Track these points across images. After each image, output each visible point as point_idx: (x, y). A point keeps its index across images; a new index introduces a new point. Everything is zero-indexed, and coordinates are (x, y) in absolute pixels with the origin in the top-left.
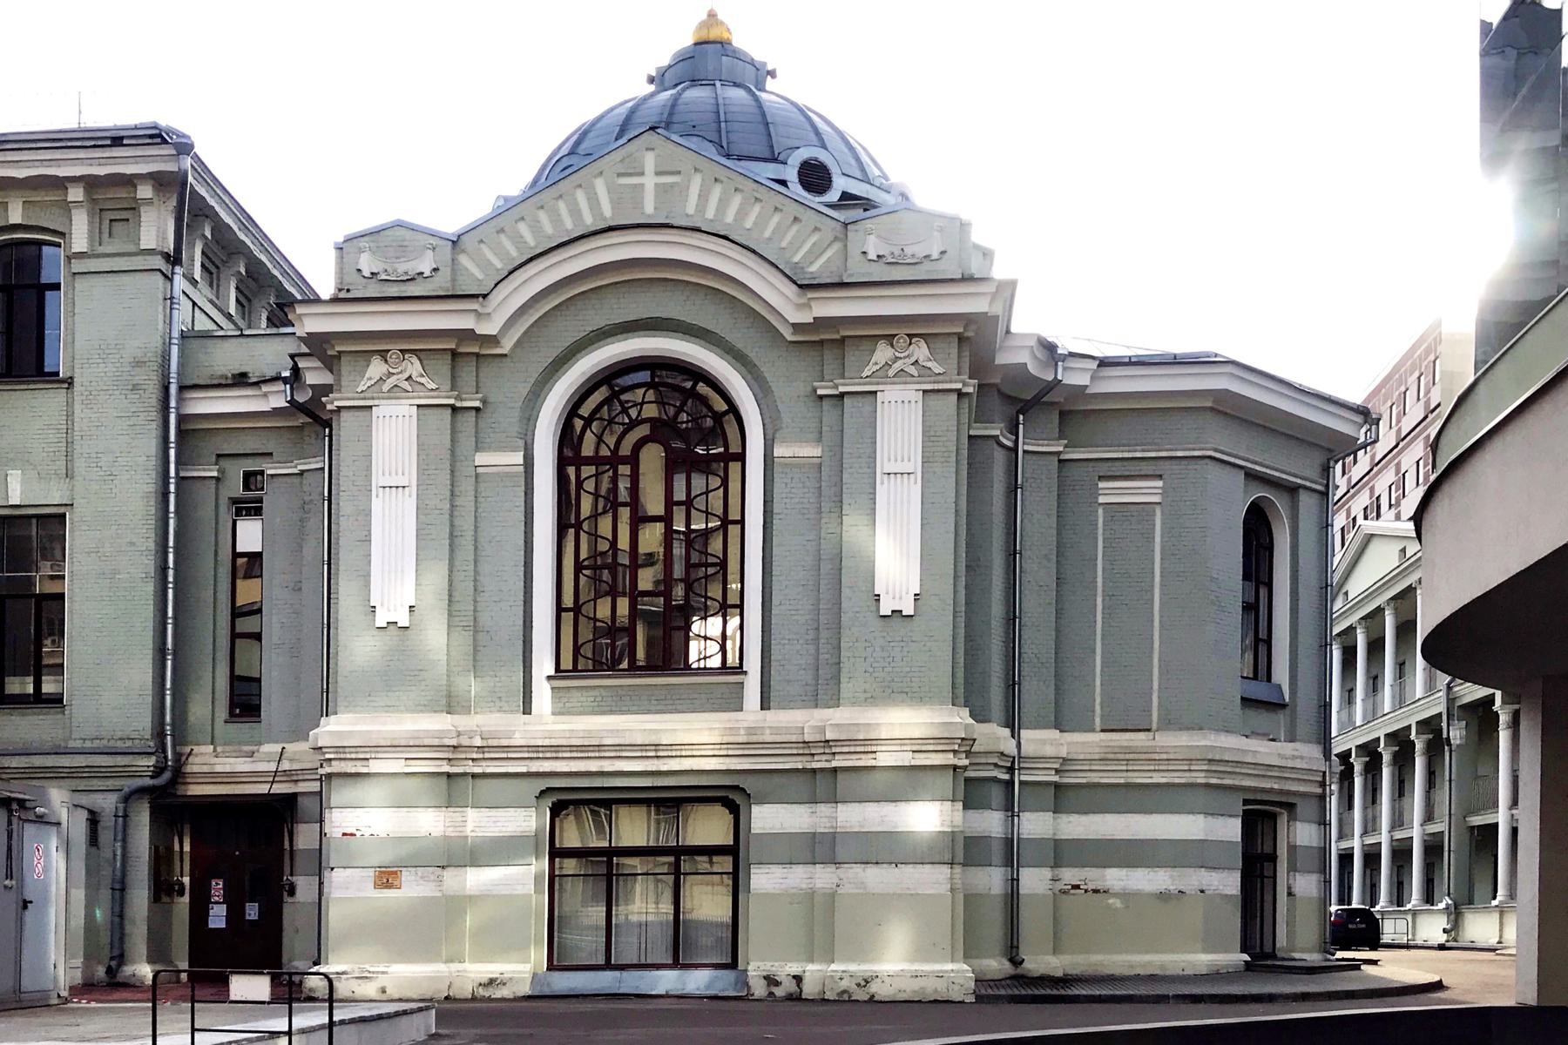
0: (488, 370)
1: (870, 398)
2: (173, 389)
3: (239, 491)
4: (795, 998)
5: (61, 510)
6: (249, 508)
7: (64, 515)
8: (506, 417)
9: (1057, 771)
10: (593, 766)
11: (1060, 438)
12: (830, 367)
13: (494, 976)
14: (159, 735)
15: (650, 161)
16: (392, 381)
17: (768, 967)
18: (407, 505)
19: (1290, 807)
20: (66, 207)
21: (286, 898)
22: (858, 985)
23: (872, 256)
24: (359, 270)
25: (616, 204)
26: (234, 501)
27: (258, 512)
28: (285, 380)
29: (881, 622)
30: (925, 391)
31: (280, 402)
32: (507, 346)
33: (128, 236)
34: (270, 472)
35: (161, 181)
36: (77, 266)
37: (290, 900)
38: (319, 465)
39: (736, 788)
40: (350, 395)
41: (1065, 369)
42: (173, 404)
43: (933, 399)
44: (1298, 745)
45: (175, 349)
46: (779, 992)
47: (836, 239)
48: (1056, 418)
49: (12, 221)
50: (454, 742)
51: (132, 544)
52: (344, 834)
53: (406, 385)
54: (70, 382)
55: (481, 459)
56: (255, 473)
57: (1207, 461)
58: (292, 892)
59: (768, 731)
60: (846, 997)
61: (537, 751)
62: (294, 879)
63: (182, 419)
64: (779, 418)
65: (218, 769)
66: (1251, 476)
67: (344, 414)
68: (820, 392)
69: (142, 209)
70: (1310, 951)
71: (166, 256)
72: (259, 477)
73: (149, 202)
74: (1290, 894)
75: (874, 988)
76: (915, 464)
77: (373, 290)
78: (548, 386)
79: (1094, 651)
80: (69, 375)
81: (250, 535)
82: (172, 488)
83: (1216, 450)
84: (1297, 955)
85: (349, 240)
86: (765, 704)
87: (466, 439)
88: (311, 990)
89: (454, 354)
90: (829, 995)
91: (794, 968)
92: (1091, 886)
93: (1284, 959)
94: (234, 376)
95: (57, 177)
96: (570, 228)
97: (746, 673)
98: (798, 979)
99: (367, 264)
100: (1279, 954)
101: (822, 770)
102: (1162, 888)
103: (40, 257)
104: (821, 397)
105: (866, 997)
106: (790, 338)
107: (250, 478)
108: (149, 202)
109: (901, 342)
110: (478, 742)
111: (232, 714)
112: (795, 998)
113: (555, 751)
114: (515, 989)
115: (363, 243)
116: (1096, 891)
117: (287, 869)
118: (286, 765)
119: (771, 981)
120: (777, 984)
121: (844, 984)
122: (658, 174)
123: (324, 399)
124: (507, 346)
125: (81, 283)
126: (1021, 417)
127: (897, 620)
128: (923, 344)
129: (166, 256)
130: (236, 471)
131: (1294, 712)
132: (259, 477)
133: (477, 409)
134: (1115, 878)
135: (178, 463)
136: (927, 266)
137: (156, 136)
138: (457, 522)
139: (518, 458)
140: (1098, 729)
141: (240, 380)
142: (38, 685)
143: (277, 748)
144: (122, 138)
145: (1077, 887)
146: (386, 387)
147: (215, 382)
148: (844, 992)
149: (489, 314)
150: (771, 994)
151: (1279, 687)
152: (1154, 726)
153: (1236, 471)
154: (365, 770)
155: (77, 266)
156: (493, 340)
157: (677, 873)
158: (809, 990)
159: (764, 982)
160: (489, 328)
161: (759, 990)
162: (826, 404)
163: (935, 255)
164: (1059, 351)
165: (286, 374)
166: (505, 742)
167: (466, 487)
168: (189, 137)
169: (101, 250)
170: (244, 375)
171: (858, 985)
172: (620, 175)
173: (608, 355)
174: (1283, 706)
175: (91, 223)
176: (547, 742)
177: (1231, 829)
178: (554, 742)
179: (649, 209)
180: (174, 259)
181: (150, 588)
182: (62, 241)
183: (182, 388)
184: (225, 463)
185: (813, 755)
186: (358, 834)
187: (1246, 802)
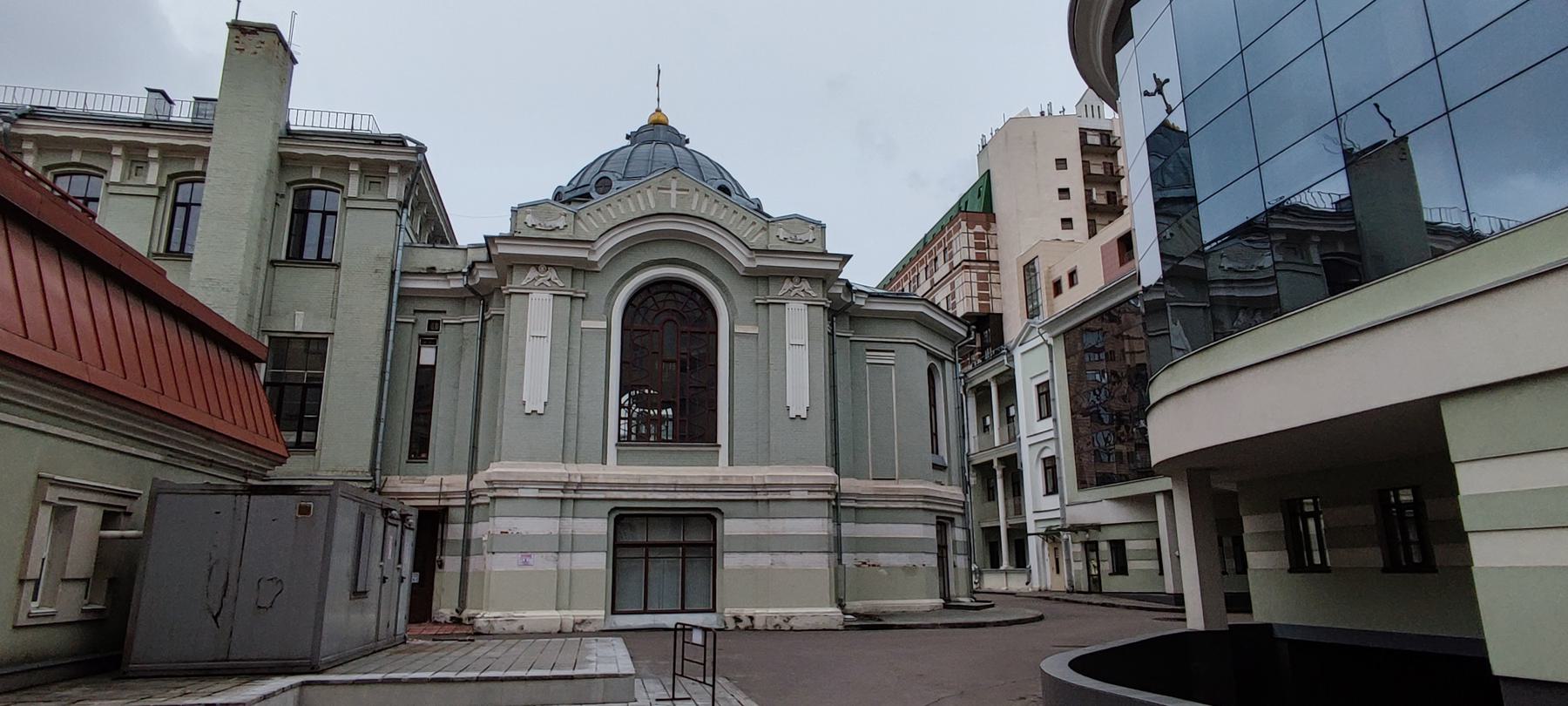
0: (590, 277)
1: (526, 296)
2: (398, 273)
3: (424, 330)
4: (750, 629)
5: (325, 336)
6: (429, 340)
7: (327, 339)
8: (598, 301)
9: (562, 490)
10: (641, 495)
11: (851, 329)
12: (762, 289)
13: (585, 618)
14: (373, 469)
15: (674, 184)
16: (540, 280)
17: (736, 611)
18: (546, 346)
19: (952, 520)
20: (348, 173)
21: (437, 569)
22: (784, 621)
23: (782, 238)
24: (526, 223)
25: (657, 202)
26: (420, 336)
27: (434, 342)
28: (464, 274)
29: (790, 421)
30: (554, 295)
31: (460, 285)
32: (600, 267)
33: (380, 190)
34: (444, 321)
35: (403, 167)
36: (112, 189)
37: (440, 570)
38: (477, 320)
39: (716, 510)
40: (516, 286)
41: (856, 297)
42: (397, 281)
43: (812, 309)
44: (953, 487)
45: (400, 252)
46: (741, 626)
47: (763, 228)
48: (848, 319)
49: (313, 177)
50: (566, 480)
51: (367, 358)
52: (502, 532)
53: (548, 283)
54: (337, 266)
55: (585, 324)
56: (435, 321)
57: (915, 346)
58: (441, 566)
59: (734, 478)
60: (778, 628)
61: (610, 486)
62: (442, 558)
63: (401, 289)
64: (736, 313)
65: (403, 490)
66: (930, 354)
67: (513, 296)
68: (757, 301)
69: (150, 163)
70: (964, 597)
71: (400, 203)
72: (437, 324)
73: (394, 175)
74: (955, 566)
75: (793, 622)
76: (547, 332)
77: (533, 233)
78: (620, 288)
79: (867, 438)
80: (338, 261)
81: (428, 356)
82: (392, 327)
83: (918, 340)
84: (961, 599)
85: (521, 207)
86: (731, 464)
87: (577, 314)
88: (479, 628)
89: (573, 270)
90: (770, 628)
91: (749, 611)
92: (871, 563)
93: (954, 602)
94: (428, 269)
95: (106, 140)
96: (644, 210)
97: (720, 446)
98: (752, 618)
99: (530, 219)
100: (953, 599)
101: (762, 500)
102: (905, 564)
103: (309, 198)
104: (757, 304)
105: (789, 628)
106: (742, 273)
107: (433, 325)
108: (394, 175)
109: (797, 280)
110: (579, 480)
111: (410, 457)
112: (750, 629)
113: (620, 486)
114: (596, 626)
115: (528, 210)
116: (874, 565)
117: (439, 553)
118: (445, 489)
119: (737, 619)
120: (741, 621)
121: (778, 621)
122: (678, 190)
123: (503, 287)
124: (600, 267)
125: (350, 213)
126: (835, 319)
127: (798, 419)
128: (807, 282)
129: (400, 203)
130: (424, 320)
131: (950, 470)
132: (437, 324)
133: (583, 298)
134: (883, 558)
135: (396, 314)
136: (807, 245)
137: (400, 141)
138: (571, 357)
139: (604, 325)
140: (871, 478)
141: (431, 271)
142: (299, 436)
143: (438, 478)
144: (380, 141)
145: (865, 563)
146: (536, 284)
147: (417, 271)
148: (777, 625)
149: (595, 251)
150: (737, 627)
151: (943, 458)
152: (897, 478)
153: (923, 350)
154: (516, 495)
155: (112, 189)
156: (595, 264)
157: (647, 557)
158: (759, 624)
159: (733, 621)
160: (595, 258)
161: (731, 625)
162: (760, 307)
163: (811, 240)
164: (853, 288)
165: (465, 270)
166: (594, 481)
167: (576, 338)
168: (423, 145)
169: (362, 196)
170: (434, 268)
171: (784, 621)
172: (659, 188)
173: (646, 277)
174: (945, 468)
175: (360, 182)
176: (617, 481)
177: (931, 532)
178: (620, 481)
179: (673, 206)
180: (404, 205)
181: (376, 383)
182: (340, 190)
183: (402, 273)
184: (420, 316)
185: (757, 492)
186: (510, 532)
187: (938, 517)
